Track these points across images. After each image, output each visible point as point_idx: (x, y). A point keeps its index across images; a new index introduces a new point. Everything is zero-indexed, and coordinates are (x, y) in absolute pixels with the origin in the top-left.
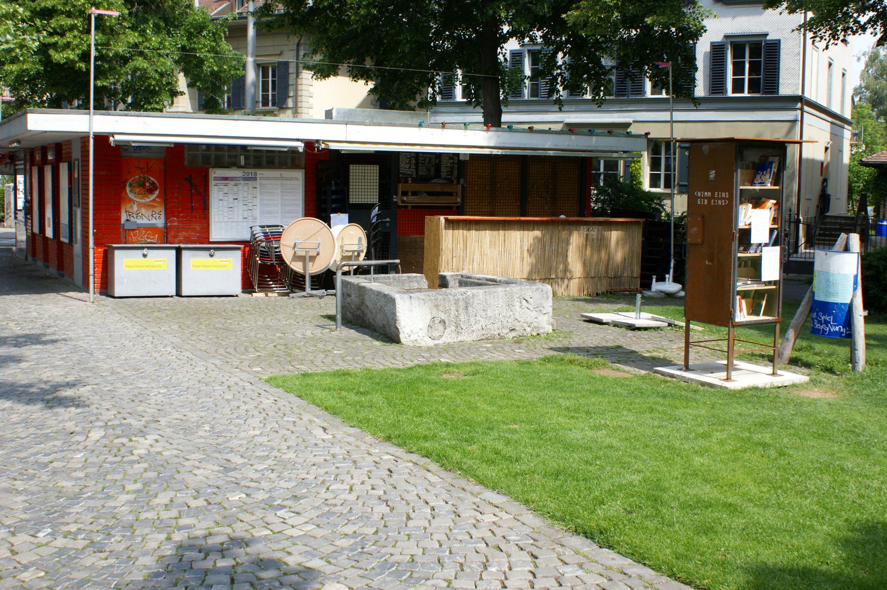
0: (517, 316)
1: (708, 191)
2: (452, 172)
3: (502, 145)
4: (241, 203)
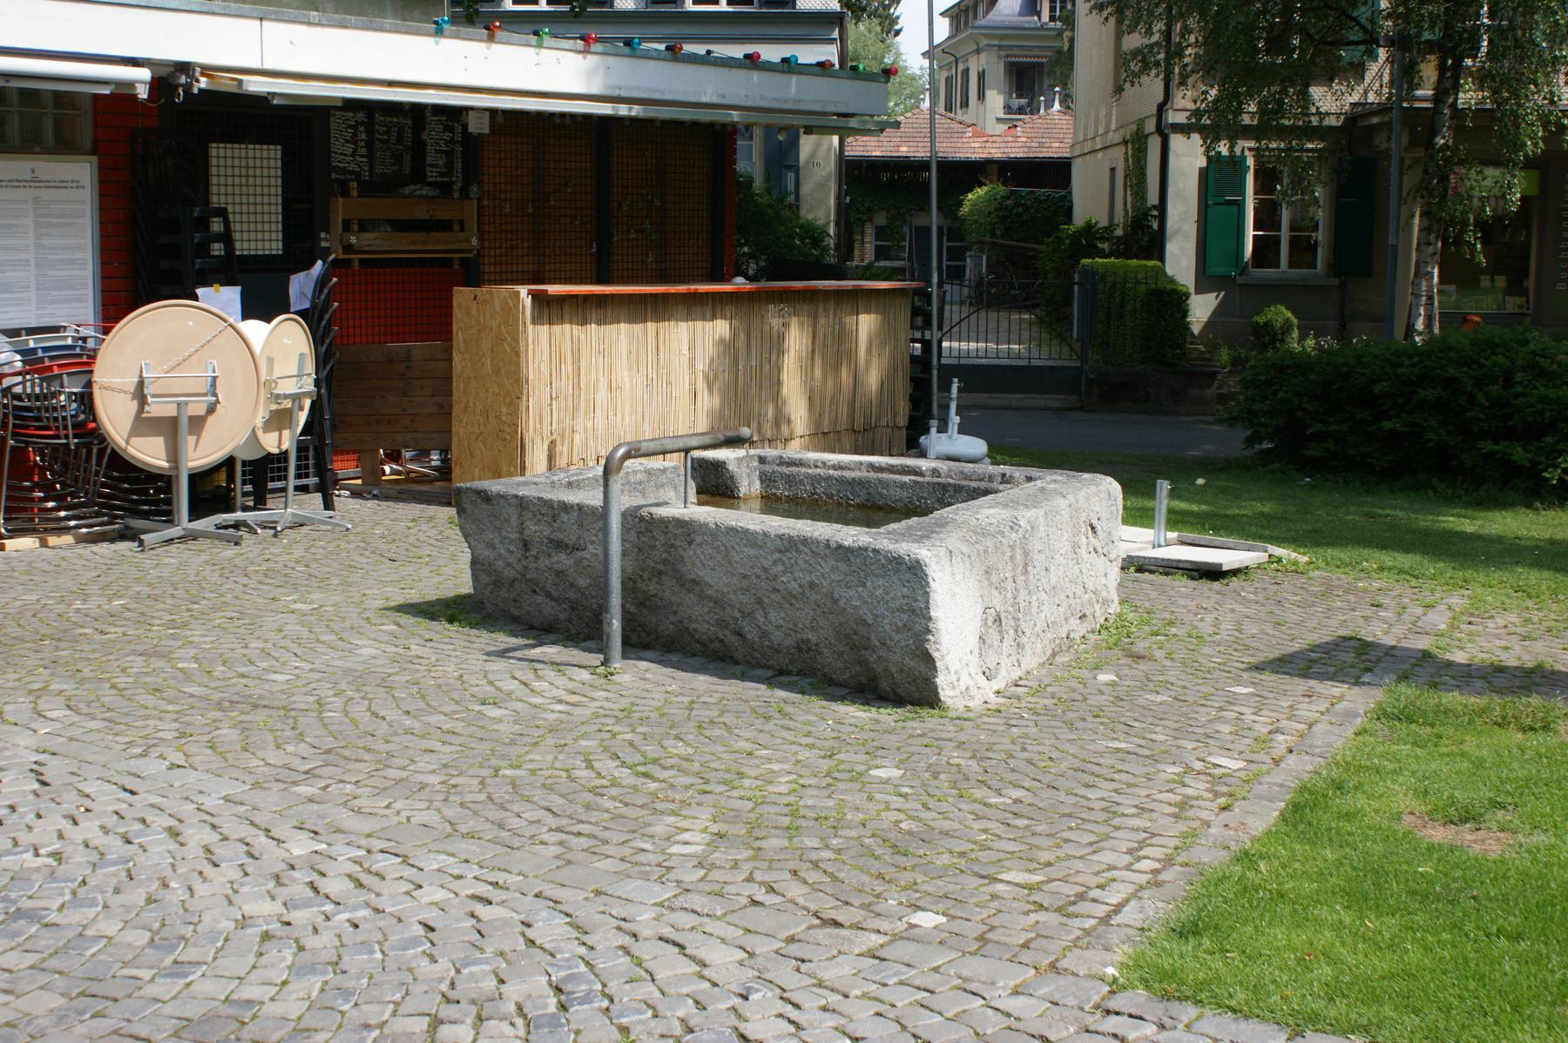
3: (615, 93)
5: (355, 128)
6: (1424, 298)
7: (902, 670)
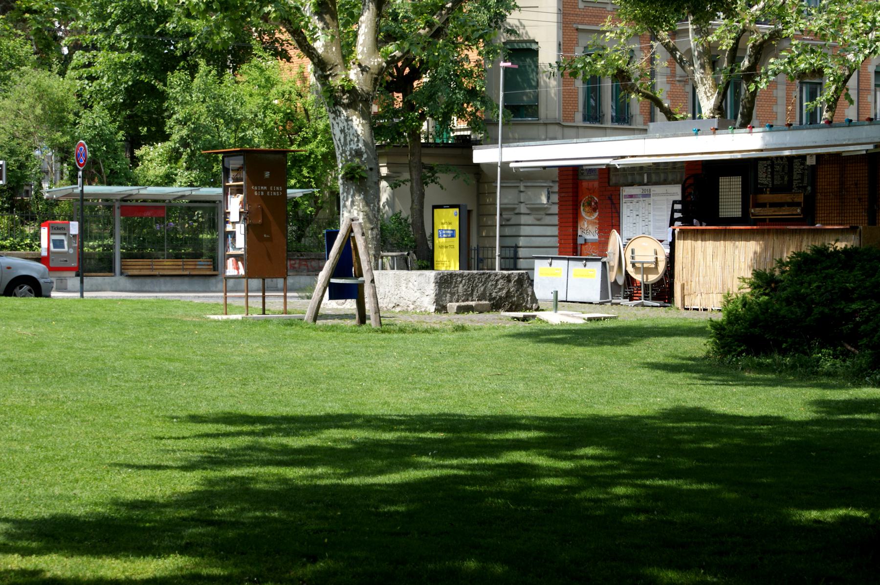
0: (403, 294)
1: (264, 186)
2: (802, 179)
4: (641, 219)
5: (767, 167)
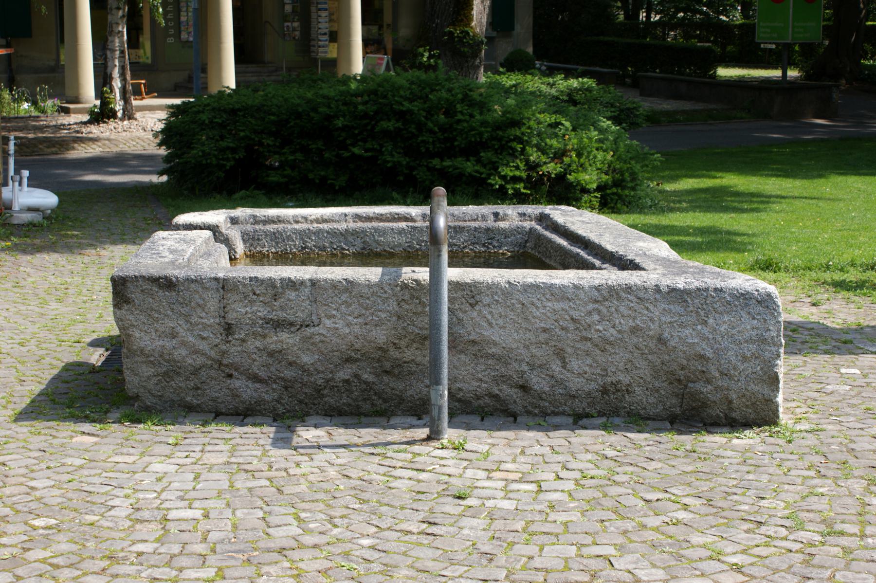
6: (118, 53)
7: (744, 395)
